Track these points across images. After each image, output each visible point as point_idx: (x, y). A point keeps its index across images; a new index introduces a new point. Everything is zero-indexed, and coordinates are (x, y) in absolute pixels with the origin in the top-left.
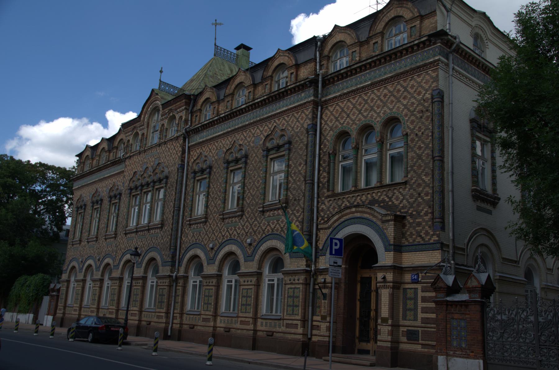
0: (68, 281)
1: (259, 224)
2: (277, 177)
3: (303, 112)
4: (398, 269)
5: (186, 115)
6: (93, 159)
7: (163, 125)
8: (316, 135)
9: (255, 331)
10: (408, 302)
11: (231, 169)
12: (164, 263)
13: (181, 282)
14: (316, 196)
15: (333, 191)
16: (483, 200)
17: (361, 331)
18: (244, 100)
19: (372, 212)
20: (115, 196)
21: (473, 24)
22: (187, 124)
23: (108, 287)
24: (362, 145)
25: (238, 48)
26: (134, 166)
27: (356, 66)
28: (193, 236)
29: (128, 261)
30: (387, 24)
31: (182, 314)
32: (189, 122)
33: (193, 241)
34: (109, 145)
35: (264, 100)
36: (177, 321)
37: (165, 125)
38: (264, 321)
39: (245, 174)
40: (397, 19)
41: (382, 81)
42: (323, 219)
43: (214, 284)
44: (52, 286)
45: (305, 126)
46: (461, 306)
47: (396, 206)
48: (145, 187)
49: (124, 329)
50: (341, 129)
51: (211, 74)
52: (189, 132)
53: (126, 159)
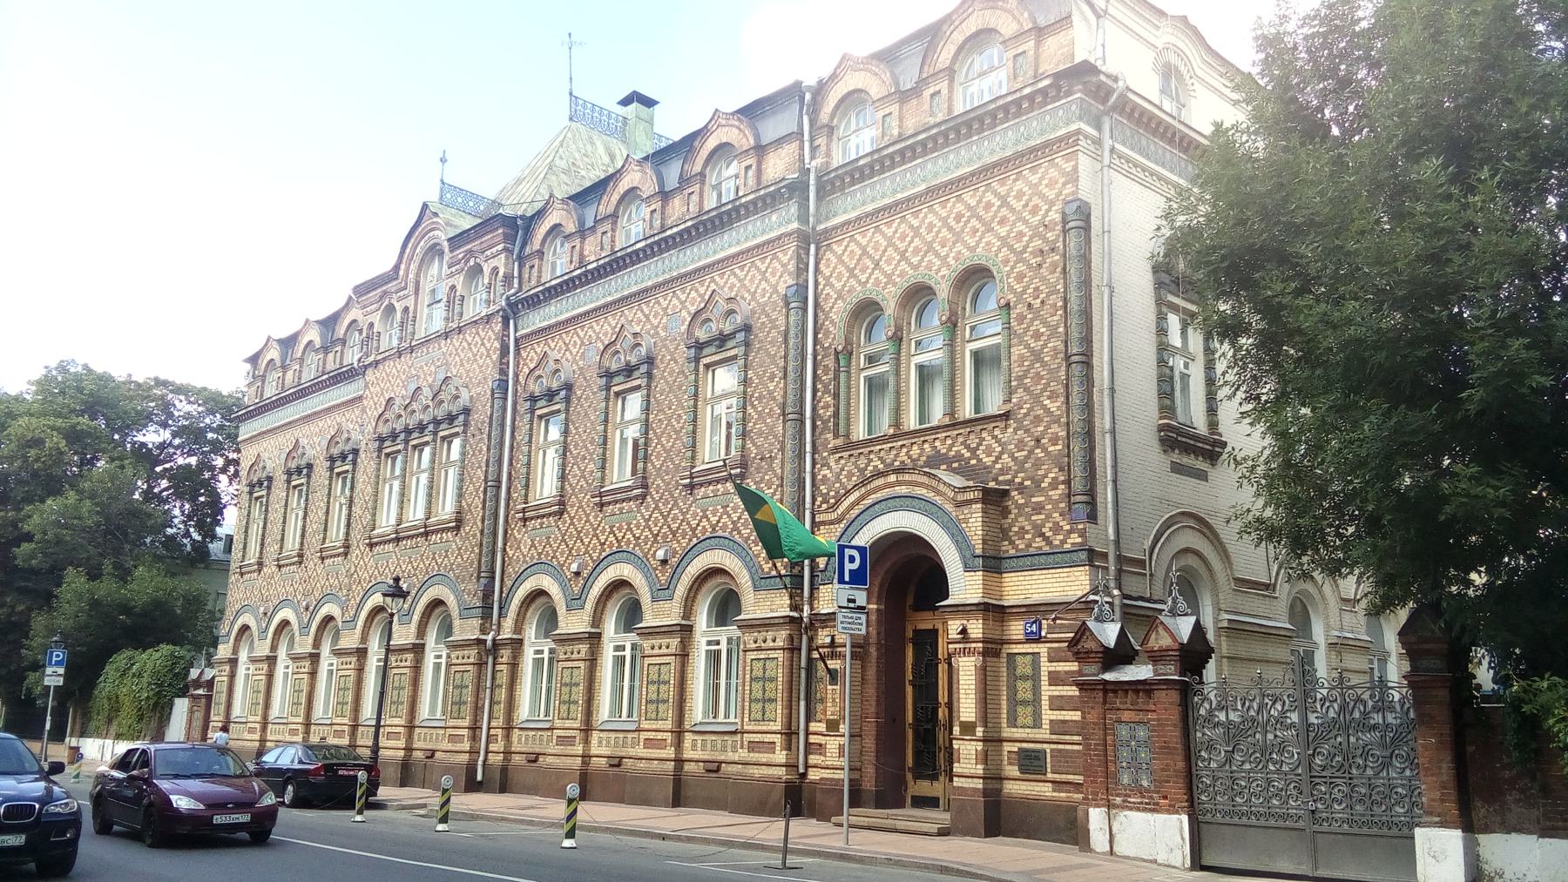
0: (233, 662)
1: (683, 514)
2: (721, 408)
3: (775, 257)
4: (994, 611)
6: (284, 368)
7: (453, 288)
8: (805, 310)
9: (679, 761)
10: (1020, 684)
11: (616, 389)
13: (505, 654)
14: (808, 448)
15: (847, 436)
16: (1187, 449)
17: (917, 754)
18: (640, 229)
19: (934, 483)
20: (343, 458)
22: (511, 286)
23: (330, 672)
25: (625, 102)
26: (390, 385)
27: (891, 150)
28: (533, 545)
29: (378, 610)
30: (960, 49)
31: (508, 729)
34: (322, 336)
35: (687, 230)
36: (498, 746)
37: (459, 288)
38: (699, 738)
40: (982, 37)
41: (951, 182)
42: (825, 501)
43: (582, 655)
44: (194, 673)
45: (782, 289)
46: (1137, 692)
48: (415, 435)
49: (369, 773)
50: (861, 296)
51: (563, 164)
52: (516, 304)
53: (366, 367)
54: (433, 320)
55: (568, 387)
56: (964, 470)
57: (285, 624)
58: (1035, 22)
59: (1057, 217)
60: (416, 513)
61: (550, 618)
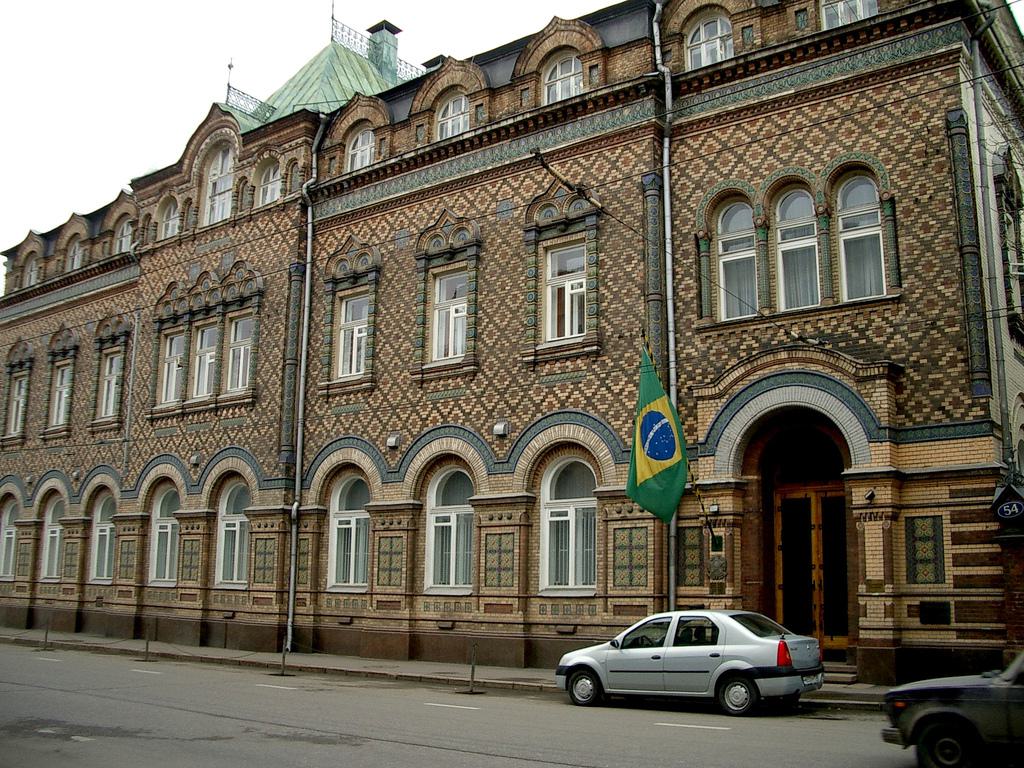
5: (305, 157)
6: (47, 259)
12: (265, 483)
13: (310, 524)
32: (314, 171)
33: (338, 433)
35: (525, 122)
37: (154, 216)
41: (822, 88)
43: (404, 525)
47: (880, 348)
54: (218, 209)
57: (53, 492)
58: (488, 83)
59: (941, 123)
60: (201, 392)
61: (173, 500)
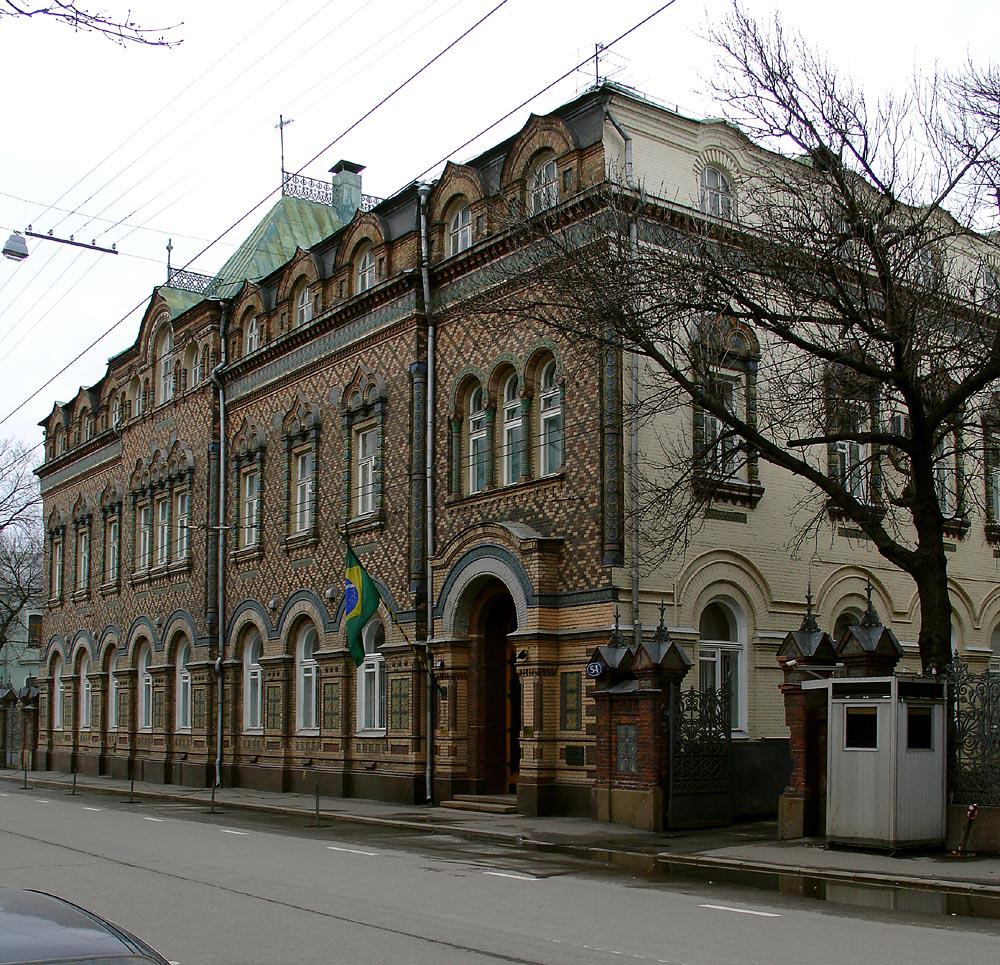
6: (68, 431)
13: (230, 674)
15: (460, 491)
21: (699, 148)
22: (219, 361)
24: (502, 403)
26: (138, 447)
33: (244, 596)
36: (229, 750)
37: (182, 363)
39: (317, 462)
43: (281, 677)
55: (263, 449)
56: (537, 524)
61: (314, 642)
